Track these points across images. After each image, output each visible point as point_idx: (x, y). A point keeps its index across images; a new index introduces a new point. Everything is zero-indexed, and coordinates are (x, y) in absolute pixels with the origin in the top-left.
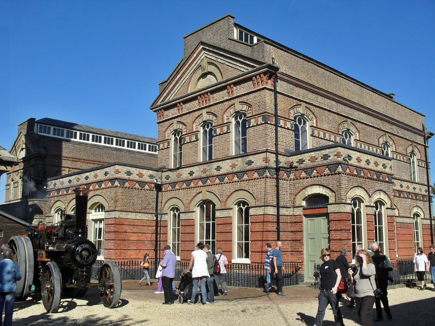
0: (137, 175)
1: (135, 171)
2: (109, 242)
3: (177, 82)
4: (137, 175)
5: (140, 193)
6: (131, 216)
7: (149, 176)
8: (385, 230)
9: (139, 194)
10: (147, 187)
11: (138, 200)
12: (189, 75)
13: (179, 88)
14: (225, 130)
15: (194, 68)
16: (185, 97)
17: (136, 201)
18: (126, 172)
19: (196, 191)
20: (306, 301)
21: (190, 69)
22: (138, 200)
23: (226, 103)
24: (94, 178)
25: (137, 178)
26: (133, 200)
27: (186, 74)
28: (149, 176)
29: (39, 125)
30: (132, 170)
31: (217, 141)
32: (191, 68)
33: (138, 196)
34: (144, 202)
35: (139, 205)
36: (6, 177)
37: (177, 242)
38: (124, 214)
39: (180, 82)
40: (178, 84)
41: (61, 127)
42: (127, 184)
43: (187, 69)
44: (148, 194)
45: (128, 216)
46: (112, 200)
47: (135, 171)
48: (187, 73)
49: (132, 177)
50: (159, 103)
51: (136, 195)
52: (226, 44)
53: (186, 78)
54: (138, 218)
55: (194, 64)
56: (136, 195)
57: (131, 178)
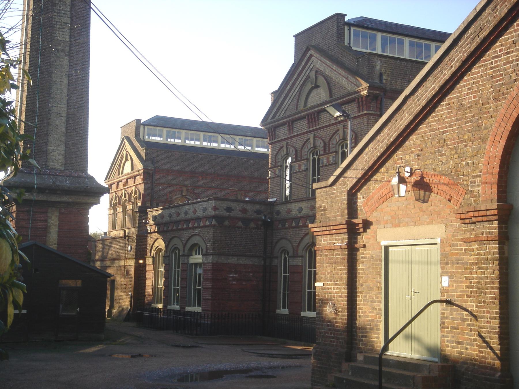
0: (240, 211)
1: (237, 207)
2: (206, 291)
3: (287, 95)
4: (240, 211)
5: (244, 232)
6: (233, 260)
7: (255, 212)
8: (305, 298)
9: (243, 234)
10: (252, 225)
11: (241, 241)
12: (299, 87)
13: (289, 103)
14: (331, 161)
15: (303, 79)
16: (293, 116)
17: (238, 243)
18: (225, 208)
19: (304, 231)
20: (476, 360)
21: (299, 80)
22: (241, 241)
23: (332, 128)
24: (193, 214)
25: (240, 215)
26: (234, 241)
27: (296, 86)
28: (255, 212)
29: (146, 127)
30: (233, 205)
31: (324, 173)
32: (300, 78)
33: (241, 236)
34: (248, 244)
35: (242, 247)
36: (271, 96)
37: (287, 292)
38: (222, 259)
39: (290, 96)
40: (288, 98)
41: (176, 128)
42: (227, 223)
43: (297, 79)
44: (253, 233)
45: (229, 261)
46: (209, 242)
47: (237, 207)
48: (297, 84)
49: (232, 214)
50: (277, 117)
51: (238, 236)
52: (334, 52)
53: (296, 91)
54: (241, 262)
55: (303, 74)
56: (238, 236)
57: (232, 215)
